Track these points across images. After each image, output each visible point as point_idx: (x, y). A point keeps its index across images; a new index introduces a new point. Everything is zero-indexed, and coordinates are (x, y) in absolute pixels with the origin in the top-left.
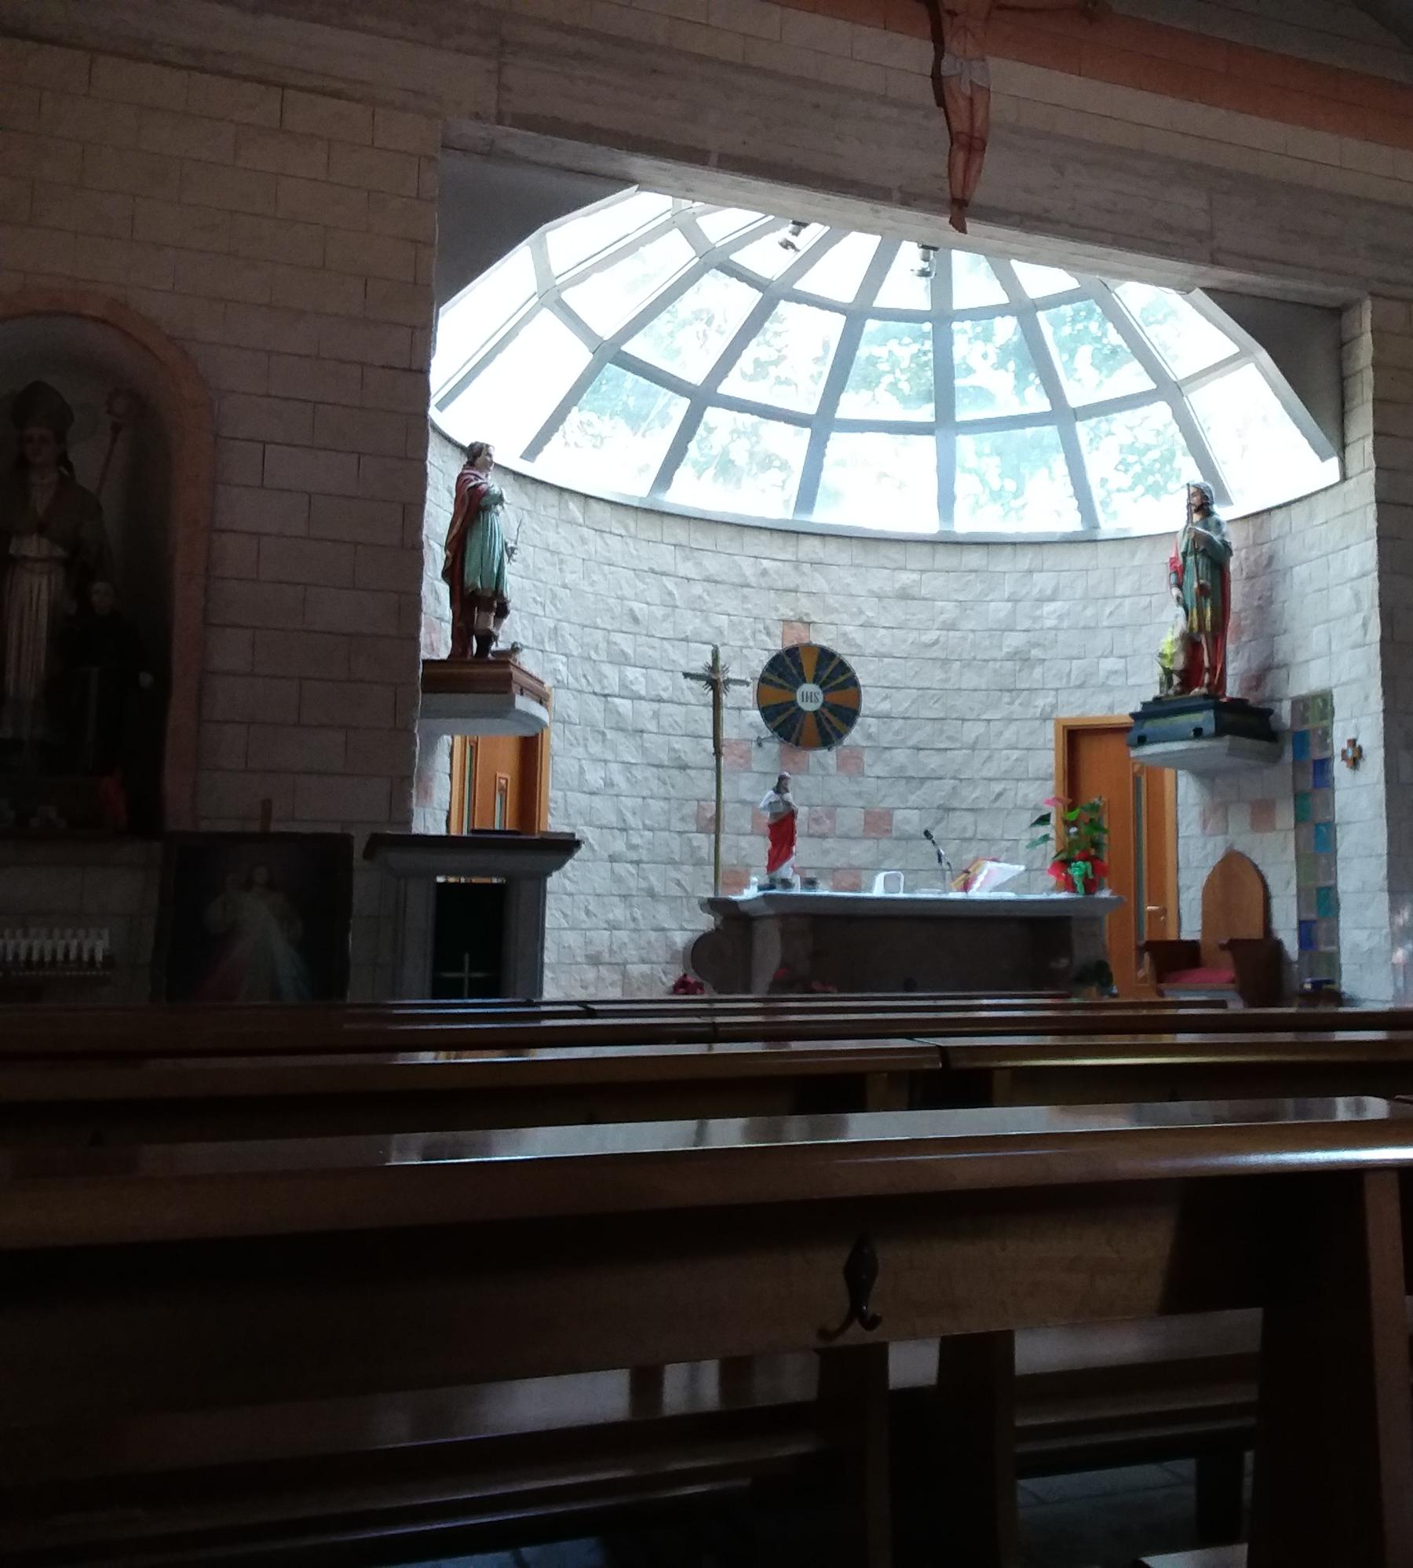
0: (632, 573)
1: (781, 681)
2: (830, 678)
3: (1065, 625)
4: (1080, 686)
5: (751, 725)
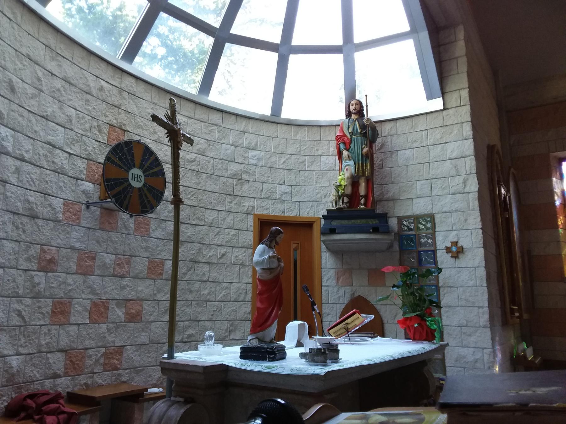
0: (14, 51)
1: (120, 163)
2: (150, 168)
3: (261, 164)
4: (267, 198)
5: (83, 192)
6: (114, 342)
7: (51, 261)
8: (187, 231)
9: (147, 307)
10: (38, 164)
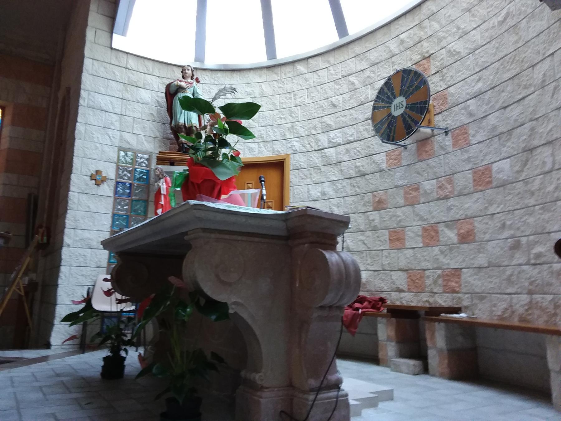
6: (448, 264)
7: (380, 202)
8: (513, 114)
9: (479, 225)
10: (361, 138)
